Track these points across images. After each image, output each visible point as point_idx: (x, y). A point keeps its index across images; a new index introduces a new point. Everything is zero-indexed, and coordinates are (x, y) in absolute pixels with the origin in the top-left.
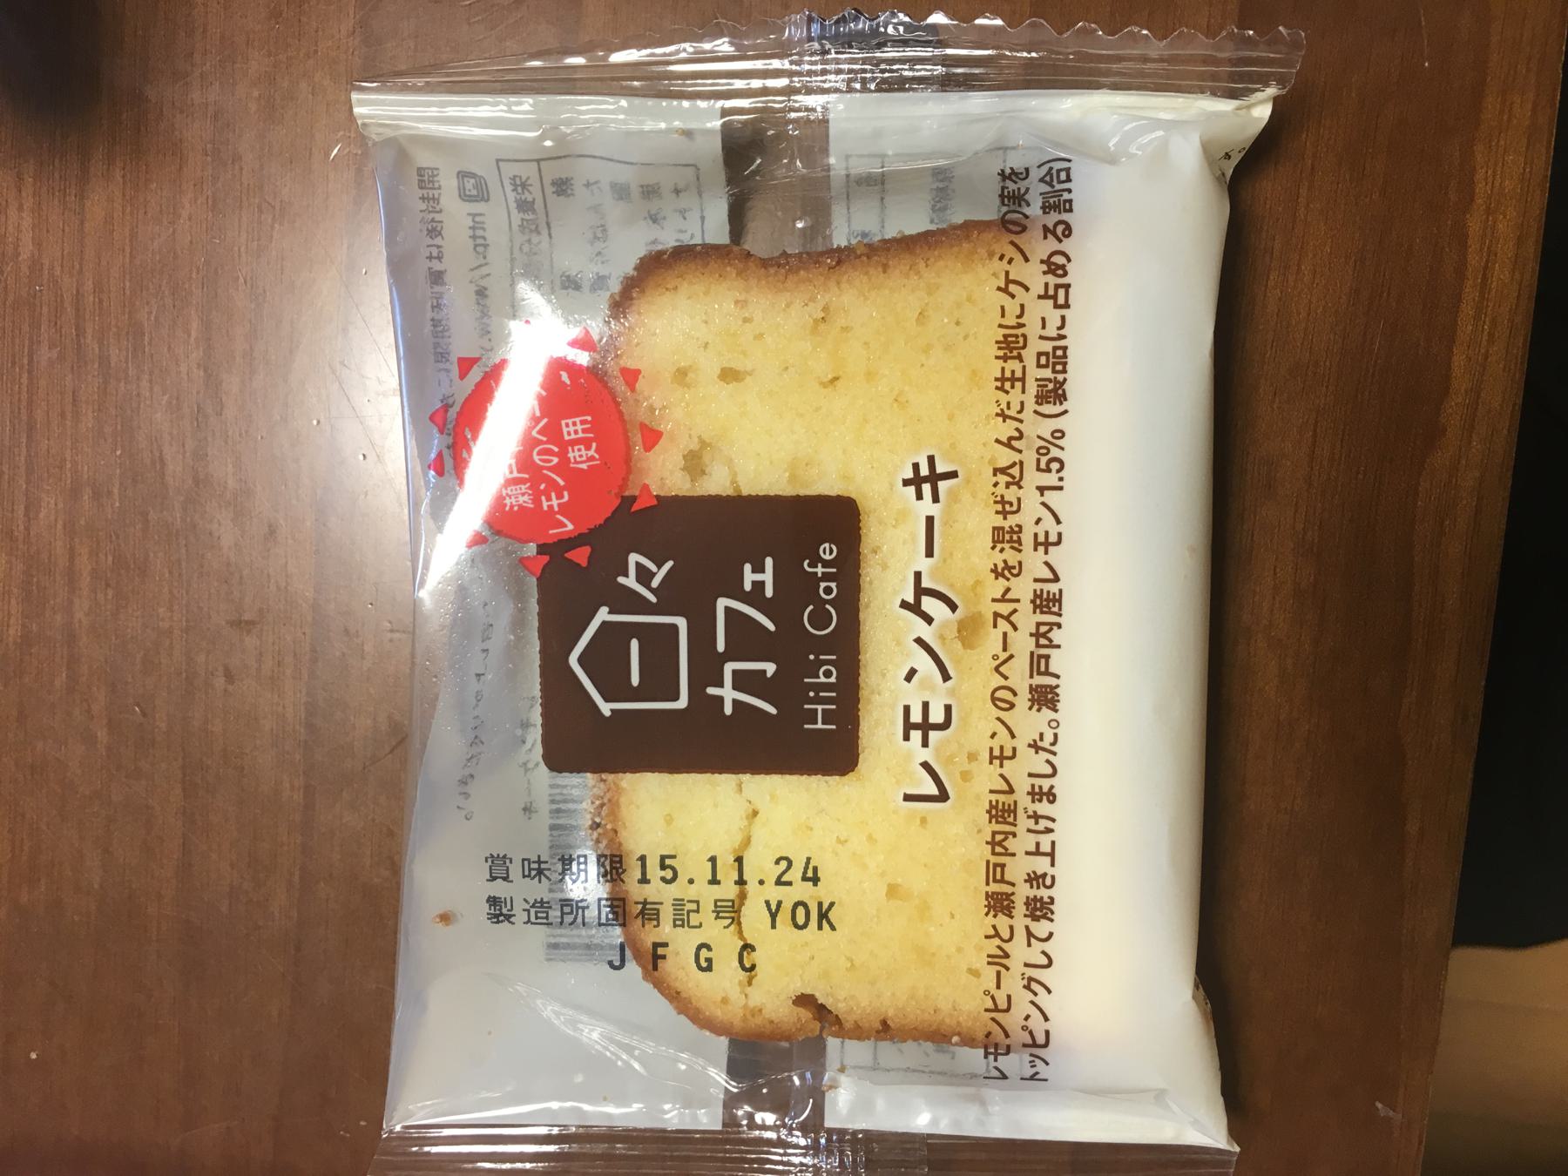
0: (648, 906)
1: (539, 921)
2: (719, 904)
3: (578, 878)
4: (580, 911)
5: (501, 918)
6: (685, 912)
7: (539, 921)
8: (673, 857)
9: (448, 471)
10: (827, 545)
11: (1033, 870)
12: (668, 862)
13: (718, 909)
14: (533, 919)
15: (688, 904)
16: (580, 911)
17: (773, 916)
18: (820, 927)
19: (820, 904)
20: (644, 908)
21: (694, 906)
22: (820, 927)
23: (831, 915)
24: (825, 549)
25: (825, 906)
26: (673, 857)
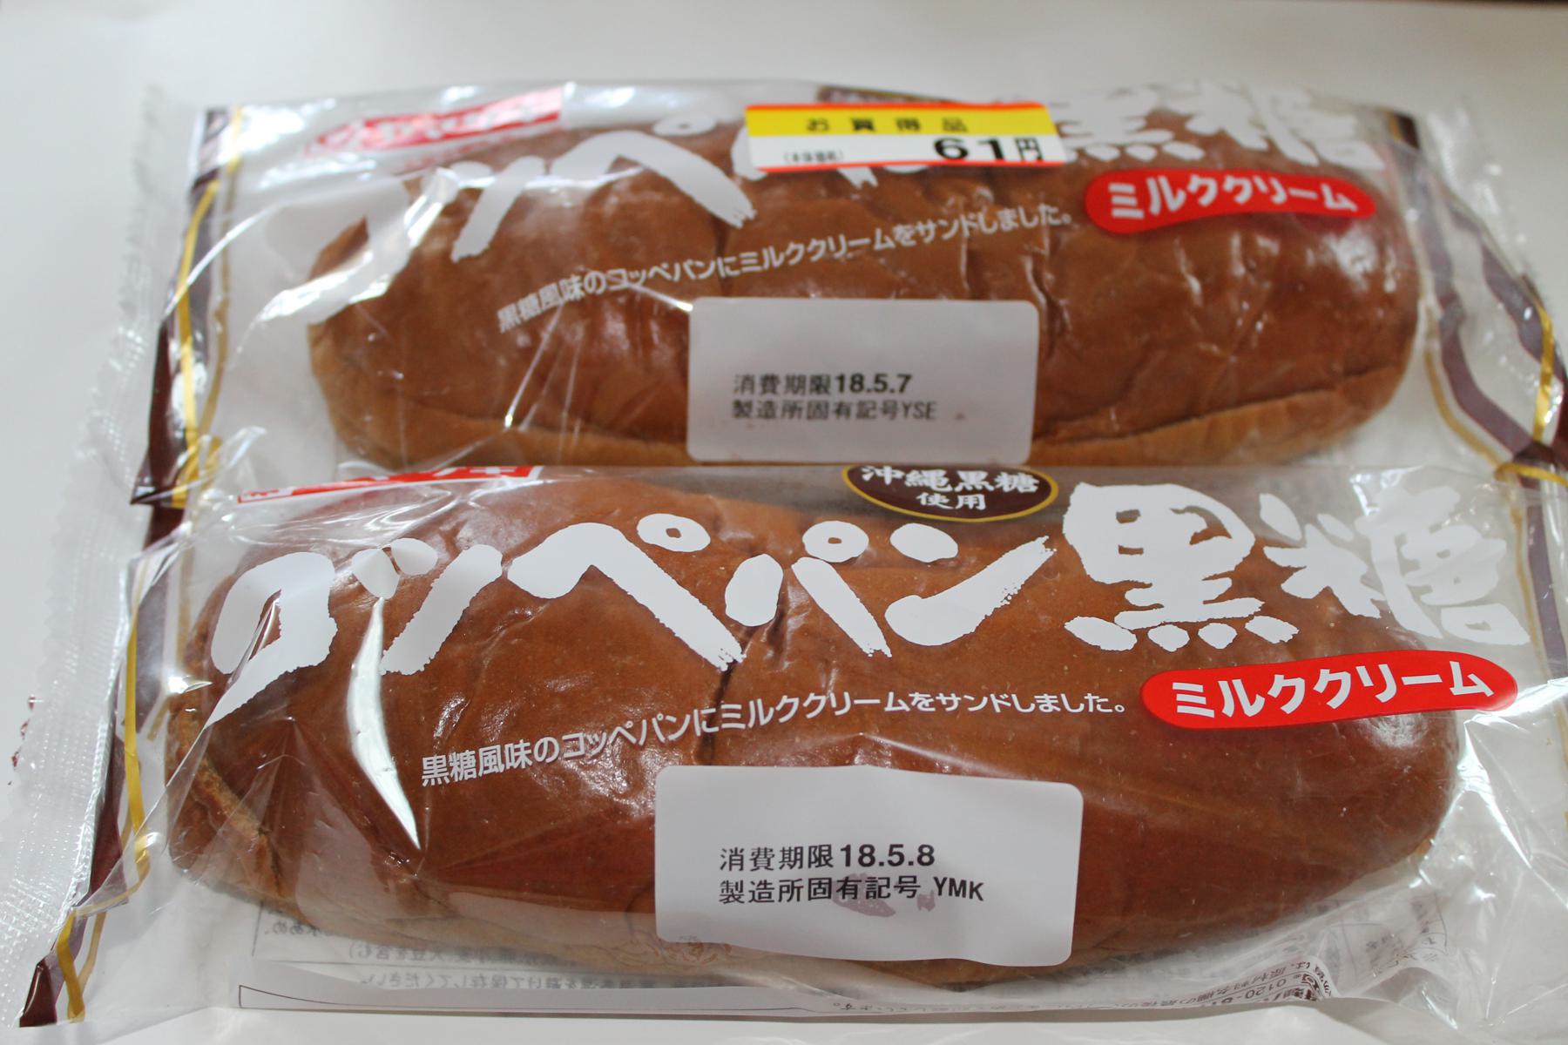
0: (849, 883)
1: (818, 895)
2: (903, 880)
3: (795, 864)
4: (796, 890)
5: (731, 899)
6: (877, 887)
7: (818, 895)
8: (901, 846)
9: (145, 866)
10: (545, 740)
11: (719, 885)
12: (895, 850)
13: (902, 885)
14: (757, 898)
15: (880, 881)
16: (796, 890)
17: (940, 887)
18: (971, 897)
19: (972, 883)
20: (845, 885)
21: (885, 882)
22: (971, 897)
23: (980, 890)
24: (542, 746)
25: (975, 886)
26: (901, 846)
